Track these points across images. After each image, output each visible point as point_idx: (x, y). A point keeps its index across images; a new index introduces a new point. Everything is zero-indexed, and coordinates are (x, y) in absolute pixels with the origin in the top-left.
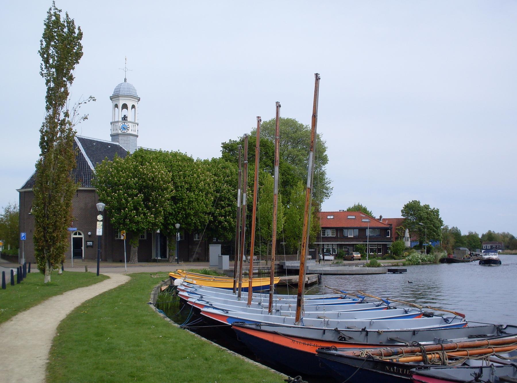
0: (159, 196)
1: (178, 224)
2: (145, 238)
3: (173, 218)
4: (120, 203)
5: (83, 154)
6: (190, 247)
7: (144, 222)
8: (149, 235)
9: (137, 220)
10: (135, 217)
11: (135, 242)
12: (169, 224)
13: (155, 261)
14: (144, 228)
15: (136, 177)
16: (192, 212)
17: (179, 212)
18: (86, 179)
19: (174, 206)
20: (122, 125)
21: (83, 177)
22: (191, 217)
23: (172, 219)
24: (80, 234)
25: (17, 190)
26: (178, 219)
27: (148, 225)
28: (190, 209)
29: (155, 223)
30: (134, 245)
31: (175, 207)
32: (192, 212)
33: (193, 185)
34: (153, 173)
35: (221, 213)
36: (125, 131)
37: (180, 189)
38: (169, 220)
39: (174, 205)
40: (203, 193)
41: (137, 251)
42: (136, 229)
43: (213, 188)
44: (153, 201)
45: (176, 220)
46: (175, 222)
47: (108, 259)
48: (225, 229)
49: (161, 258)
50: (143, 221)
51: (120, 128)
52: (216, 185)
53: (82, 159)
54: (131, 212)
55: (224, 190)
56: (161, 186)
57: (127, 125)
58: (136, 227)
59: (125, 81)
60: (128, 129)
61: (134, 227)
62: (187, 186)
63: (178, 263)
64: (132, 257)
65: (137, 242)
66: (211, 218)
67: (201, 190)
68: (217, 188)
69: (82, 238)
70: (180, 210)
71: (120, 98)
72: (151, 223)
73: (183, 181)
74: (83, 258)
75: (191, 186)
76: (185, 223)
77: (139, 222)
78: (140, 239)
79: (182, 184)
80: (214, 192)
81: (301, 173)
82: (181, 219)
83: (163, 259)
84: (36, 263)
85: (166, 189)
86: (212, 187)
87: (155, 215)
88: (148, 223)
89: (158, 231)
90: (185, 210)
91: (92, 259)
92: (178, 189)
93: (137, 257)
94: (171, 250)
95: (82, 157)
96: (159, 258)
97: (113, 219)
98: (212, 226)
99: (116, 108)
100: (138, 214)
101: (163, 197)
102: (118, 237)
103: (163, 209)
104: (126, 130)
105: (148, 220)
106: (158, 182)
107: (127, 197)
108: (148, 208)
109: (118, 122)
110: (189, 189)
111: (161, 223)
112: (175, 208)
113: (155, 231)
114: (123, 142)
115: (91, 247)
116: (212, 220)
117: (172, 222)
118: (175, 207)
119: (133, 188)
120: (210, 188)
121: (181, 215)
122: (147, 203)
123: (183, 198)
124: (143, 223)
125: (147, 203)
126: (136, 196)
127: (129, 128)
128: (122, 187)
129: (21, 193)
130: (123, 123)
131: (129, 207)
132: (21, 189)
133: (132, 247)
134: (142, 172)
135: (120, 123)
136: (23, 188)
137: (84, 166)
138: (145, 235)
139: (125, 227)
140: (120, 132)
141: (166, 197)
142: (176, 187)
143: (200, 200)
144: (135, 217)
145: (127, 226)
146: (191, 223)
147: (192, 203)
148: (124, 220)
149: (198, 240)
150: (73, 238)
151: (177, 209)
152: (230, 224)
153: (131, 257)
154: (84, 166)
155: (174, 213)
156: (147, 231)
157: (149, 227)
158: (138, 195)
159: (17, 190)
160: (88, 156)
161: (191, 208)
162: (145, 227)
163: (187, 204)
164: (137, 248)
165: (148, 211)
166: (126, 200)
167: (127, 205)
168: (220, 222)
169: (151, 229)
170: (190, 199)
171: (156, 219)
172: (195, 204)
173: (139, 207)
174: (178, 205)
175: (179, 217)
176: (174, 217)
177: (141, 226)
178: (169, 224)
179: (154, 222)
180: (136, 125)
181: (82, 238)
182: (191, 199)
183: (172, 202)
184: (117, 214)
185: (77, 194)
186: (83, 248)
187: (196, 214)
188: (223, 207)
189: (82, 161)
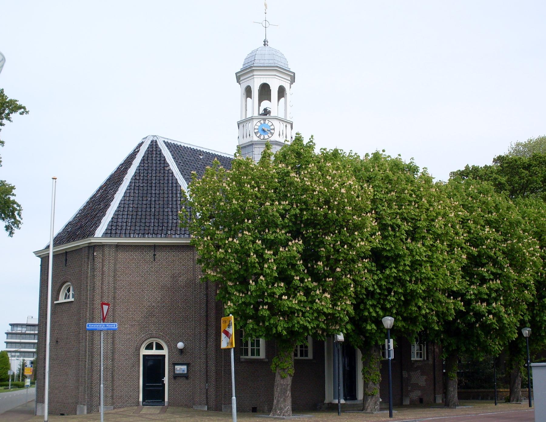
0: (343, 243)
1: (390, 318)
2: (310, 356)
3: (375, 303)
4: (246, 262)
5: (172, 173)
6: (405, 374)
7: (308, 312)
8: (319, 347)
9: (289, 308)
10: (284, 297)
11: (286, 365)
12: (365, 320)
13: (333, 408)
14: (305, 328)
15: (285, 197)
16: (421, 288)
17: (389, 290)
18: (175, 221)
19: (378, 275)
20: (259, 124)
21: (170, 217)
22: (416, 300)
23: (373, 306)
24: (159, 347)
26: (388, 306)
27: (317, 318)
28: (416, 283)
29: (333, 315)
30: (282, 372)
31: (381, 276)
32: (421, 288)
33: (422, 224)
34: (327, 185)
35: (480, 293)
37: (391, 233)
38: (366, 309)
39: (379, 272)
40: (442, 244)
41: (289, 388)
42: (287, 329)
43: (463, 235)
44: (328, 258)
45: (384, 309)
46: (381, 313)
47: (223, 406)
48: (487, 328)
49: (345, 399)
50: (303, 309)
51: (256, 131)
52: (470, 229)
53: (170, 182)
54: (273, 285)
55: (487, 238)
56: (348, 220)
57: (270, 124)
58: (286, 326)
59: (265, 45)
60: (272, 131)
61: (282, 326)
62: (406, 227)
63: (391, 416)
64: (278, 401)
65: (289, 364)
66: (461, 306)
67: (437, 237)
68: (471, 236)
69: (165, 355)
70: (392, 283)
71: (255, 73)
72: (324, 314)
73: (397, 213)
74: (166, 404)
75: (416, 228)
76: (402, 316)
77: (294, 313)
78: (299, 357)
79: (394, 221)
80: (465, 243)
82: (394, 306)
83: (349, 402)
85: (359, 227)
86: (461, 231)
87: (332, 295)
88: (315, 315)
89: (341, 337)
90: (403, 284)
91: (187, 406)
92: (386, 234)
93: (289, 401)
94: (371, 383)
95: (170, 178)
96: (342, 401)
97: (229, 304)
98: (459, 323)
99: (248, 99)
100: (291, 291)
101: (351, 247)
102: (247, 355)
103: (354, 280)
104: (267, 134)
105: (315, 307)
106: (340, 209)
107: (262, 248)
108: (316, 277)
109: (252, 119)
110: (413, 235)
111: (348, 314)
112: (380, 280)
113: (332, 336)
115: (185, 376)
116: (463, 309)
117: (374, 314)
118: (381, 276)
119: (277, 226)
120: (457, 234)
121: (394, 296)
122: (312, 266)
123: (399, 256)
124: (303, 313)
125: (312, 266)
126: (286, 245)
128: (250, 221)
130: (262, 122)
131: (268, 271)
133: (278, 378)
134: (301, 184)
135: (255, 122)
137: (174, 196)
138: (310, 344)
139: (258, 325)
140: (255, 139)
141: (361, 247)
142: (383, 227)
143: (439, 260)
144: (284, 297)
145: (264, 323)
146: (417, 317)
147: (418, 267)
148: (256, 309)
149: (419, 359)
150: (144, 356)
151: (386, 282)
152: (500, 319)
153: (275, 401)
154: (174, 196)
155: (378, 291)
156: (315, 335)
157: (318, 326)
158: (290, 243)
159: (36, 253)
160: (184, 177)
161: (417, 278)
162: (308, 325)
163: (408, 268)
164: (289, 380)
165: (315, 284)
166: (260, 255)
167: (262, 269)
168: (479, 315)
169: (323, 330)
170: (413, 256)
171: (335, 305)
172: (427, 270)
173: (293, 274)
174: (388, 272)
175: (390, 302)
176: (379, 303)
177: (298, 323)
178: (365, 320)
179: (330, 311)
180: (289, 126)
181: (165, 355)
182: (418, 258)
183: (373, 264)
184: (239, 291)
185: (155, 255)
186: (166, 380)
187: (429, 293)
188: (483, 281)
189: (170, 185)
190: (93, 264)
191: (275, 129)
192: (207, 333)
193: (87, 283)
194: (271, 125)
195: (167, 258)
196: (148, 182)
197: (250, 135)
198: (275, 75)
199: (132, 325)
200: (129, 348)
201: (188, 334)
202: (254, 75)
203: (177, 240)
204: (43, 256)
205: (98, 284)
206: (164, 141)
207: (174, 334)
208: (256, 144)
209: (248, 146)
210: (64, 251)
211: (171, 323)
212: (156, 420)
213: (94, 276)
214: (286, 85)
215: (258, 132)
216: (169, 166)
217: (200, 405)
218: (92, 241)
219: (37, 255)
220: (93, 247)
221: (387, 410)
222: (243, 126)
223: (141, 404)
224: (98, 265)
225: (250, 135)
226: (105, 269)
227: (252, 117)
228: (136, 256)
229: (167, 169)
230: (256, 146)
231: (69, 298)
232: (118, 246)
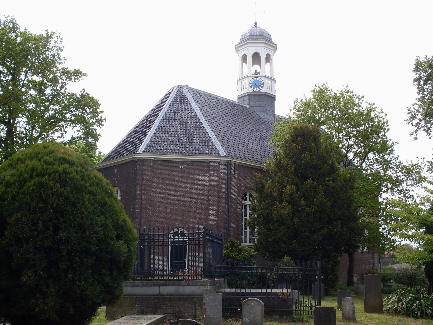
20: (253, 80)
81: (411, 242)
99: (244, 64)
127: (263, 84)
130: (255, 79)
136: (196, 93)
212: (123, 323)
214: (271, 53)
215: (252, 86)
218: (136, 156)
222: (241, 82)
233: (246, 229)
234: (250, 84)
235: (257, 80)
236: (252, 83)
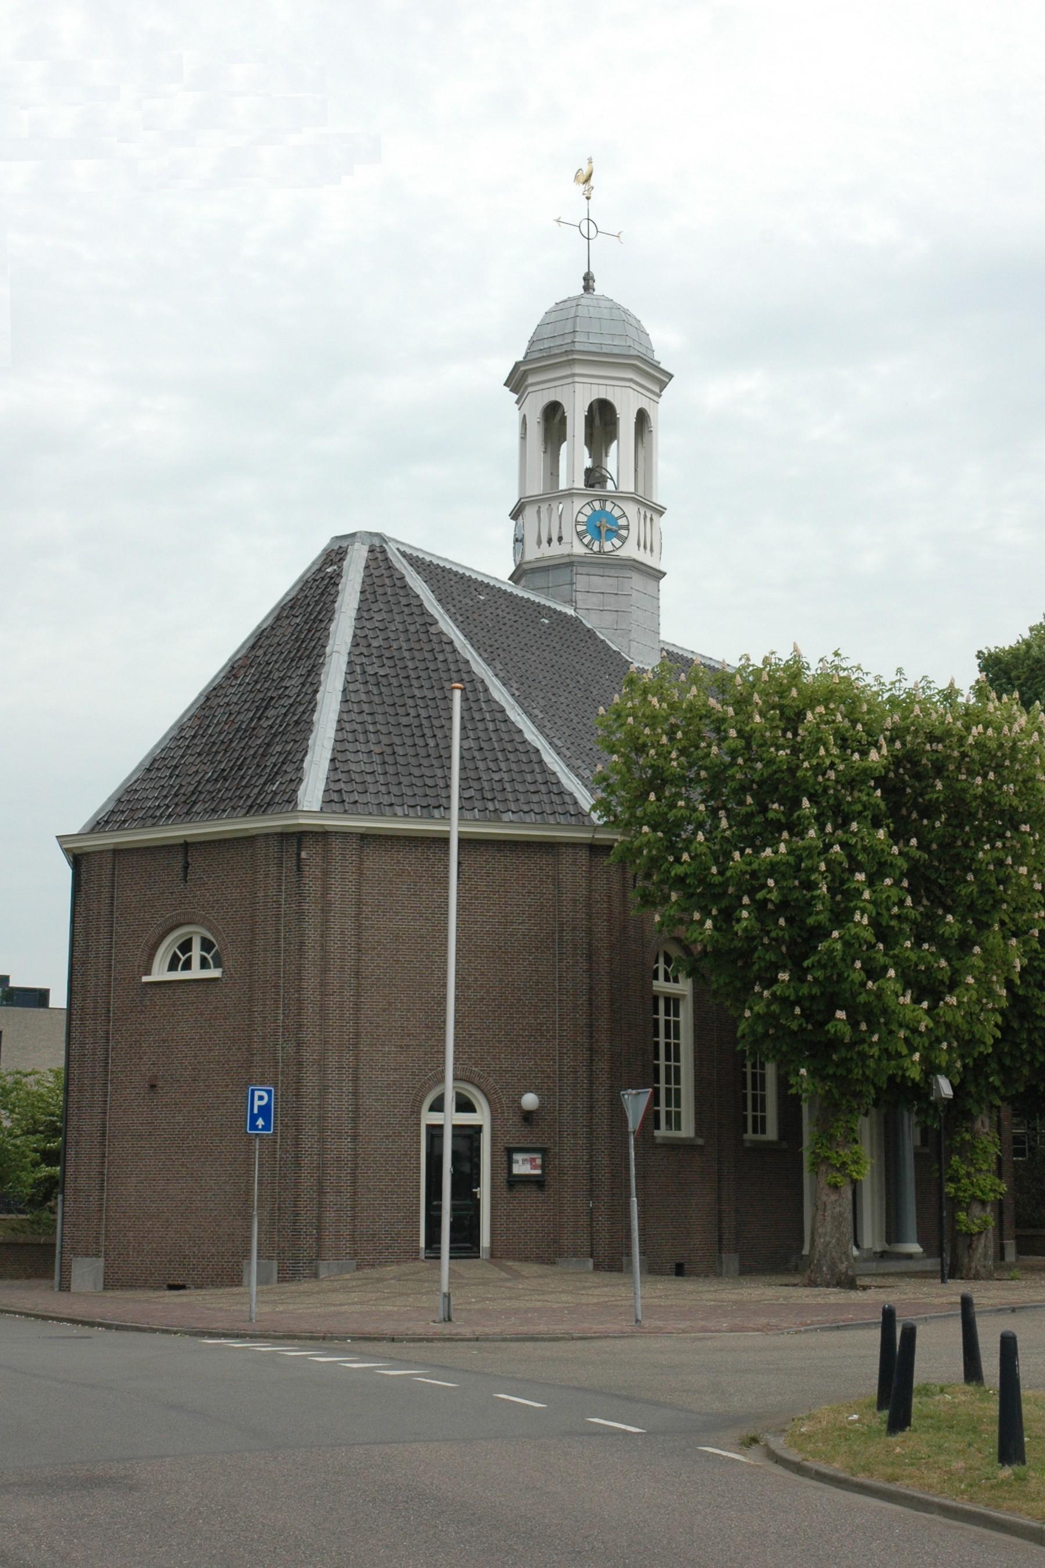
2: (772, 1133)
20: (588, 511)
25: (953, 679)
36: (608, 547)
51: (580, 528)
60: (624, 533)
69: (478, 1129)
71: (578, 370)
74: (484, 1254)
84: (182, 1287)
114: (593, 601)
115: (537, 1183)
129: (78, 860)
130: (597, 505)
132: (92, 831)
136: (100, 824)
140: (579, 549)
159: (952, 685)
181: (478, 1129)
190: (299, 884)
191: (630, 527)
192: (591, 1070)
193: (278, 931)
194: (620, 517)
195: (488, 874)
196: (396, 665)
197: (560, 539)
198: (631, 380)
199: (401, 1047)
200: (395, 1107)
201: (543, 1072)
202: (574, 375)
203: (515, 828)
204: (77, 852)
205: (312, 935)
206: (398, 549)
207: (507, 1072)
208: (582, 564)
209: (557, 567)
210: (182, 841)
211: (500, 1042)
213: (301, 914)
215: (586, 531)
216: (436, 622)
217: (575, 1256)
218: (301, 821)
219: (65, 846)
220: (299, 837)
221: (934, 1278)
223: (422, 1255)
224: (312, 886)
225: (560, 539)
226: (334, 895)
227: (570, 489)
228: (410, 866)
229: (432, 630)
230: (580, 570)
231: (187, 966)
232: (366, 838)
233: (752, 1073)
234: (577, 523)
235: (603, 509)
236: (585, 519)
